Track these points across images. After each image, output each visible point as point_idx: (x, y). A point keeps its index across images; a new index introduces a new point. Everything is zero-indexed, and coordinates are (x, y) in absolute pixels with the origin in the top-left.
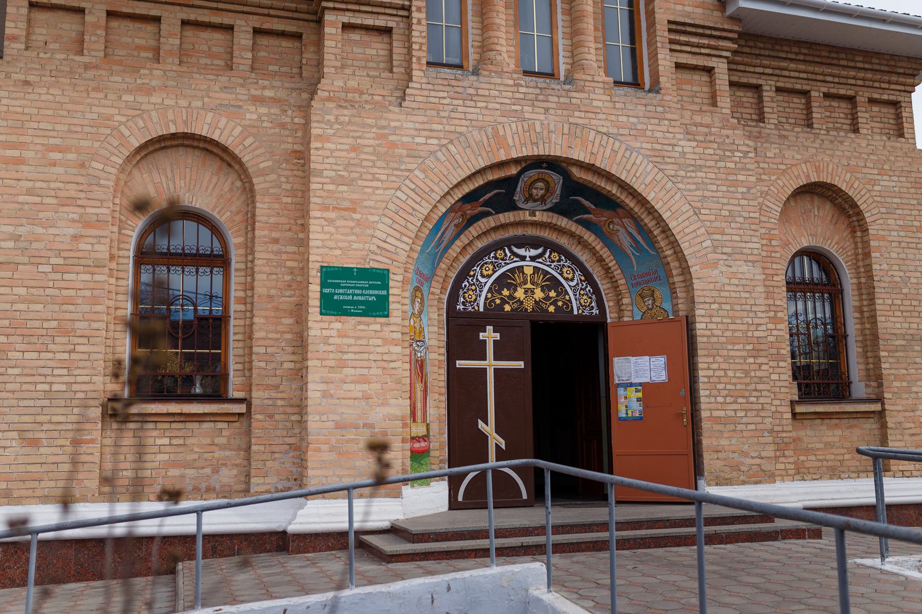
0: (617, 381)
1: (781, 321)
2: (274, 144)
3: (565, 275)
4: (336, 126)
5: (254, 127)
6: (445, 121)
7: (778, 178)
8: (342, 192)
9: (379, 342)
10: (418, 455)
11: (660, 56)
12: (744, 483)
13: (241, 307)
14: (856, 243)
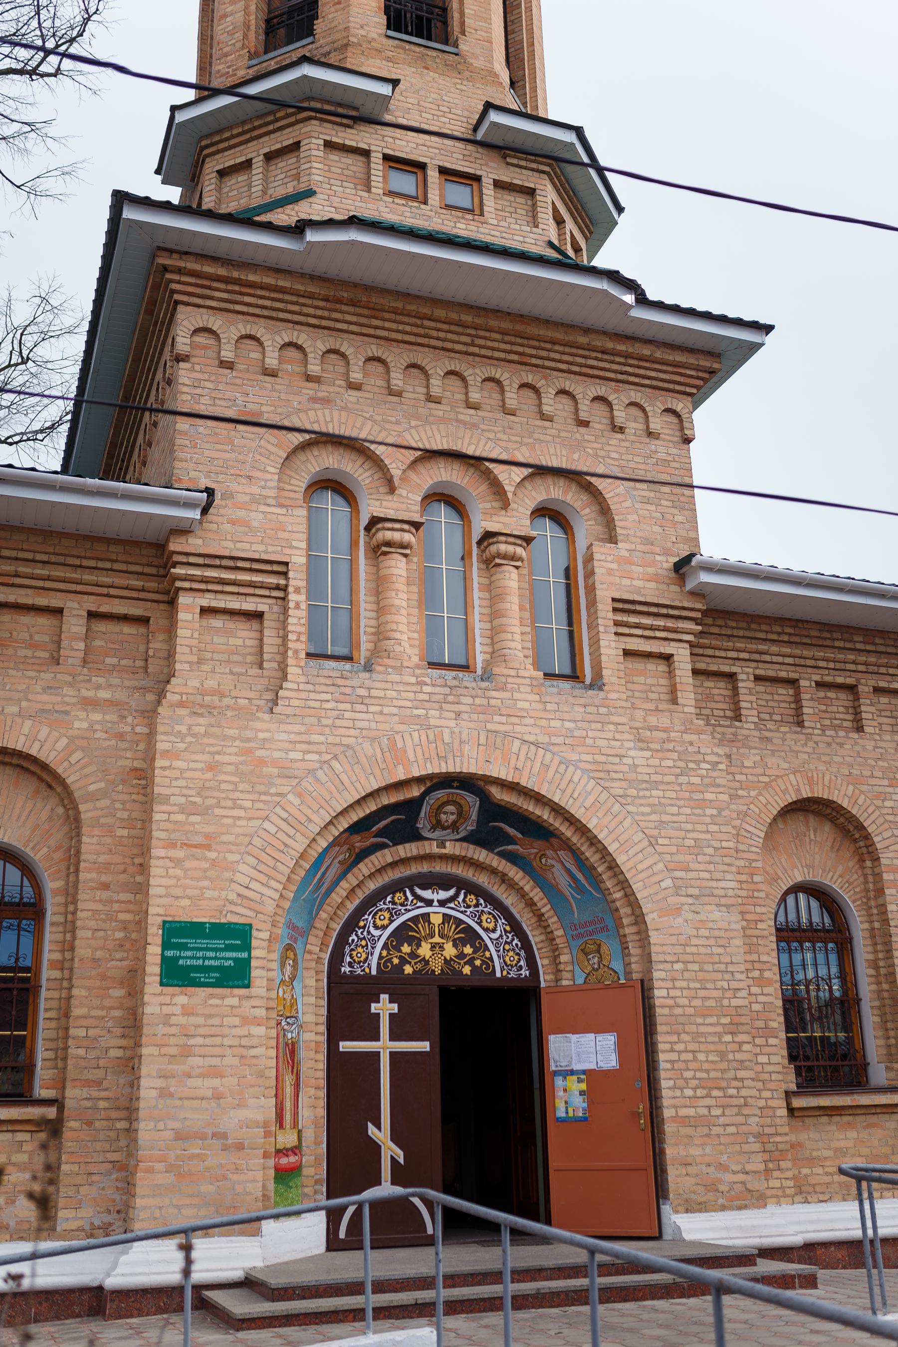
0: (553, 1068)
1: (769, 982)
2: (108, 760)
3: (485, 924)
4: (189, 739)
5: (83, 738)
6: (327, 730)
7: (760, 794)
8: (193, 824)
9: (237, 1021)
10: (285, 1175)
11: (602, 643)
12: (723, 1208)
13: (57, 974)
14: (865, 876)
